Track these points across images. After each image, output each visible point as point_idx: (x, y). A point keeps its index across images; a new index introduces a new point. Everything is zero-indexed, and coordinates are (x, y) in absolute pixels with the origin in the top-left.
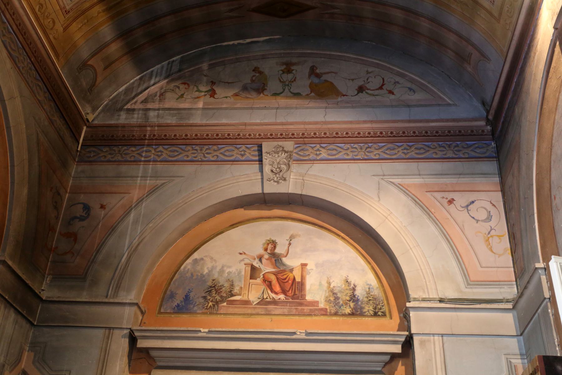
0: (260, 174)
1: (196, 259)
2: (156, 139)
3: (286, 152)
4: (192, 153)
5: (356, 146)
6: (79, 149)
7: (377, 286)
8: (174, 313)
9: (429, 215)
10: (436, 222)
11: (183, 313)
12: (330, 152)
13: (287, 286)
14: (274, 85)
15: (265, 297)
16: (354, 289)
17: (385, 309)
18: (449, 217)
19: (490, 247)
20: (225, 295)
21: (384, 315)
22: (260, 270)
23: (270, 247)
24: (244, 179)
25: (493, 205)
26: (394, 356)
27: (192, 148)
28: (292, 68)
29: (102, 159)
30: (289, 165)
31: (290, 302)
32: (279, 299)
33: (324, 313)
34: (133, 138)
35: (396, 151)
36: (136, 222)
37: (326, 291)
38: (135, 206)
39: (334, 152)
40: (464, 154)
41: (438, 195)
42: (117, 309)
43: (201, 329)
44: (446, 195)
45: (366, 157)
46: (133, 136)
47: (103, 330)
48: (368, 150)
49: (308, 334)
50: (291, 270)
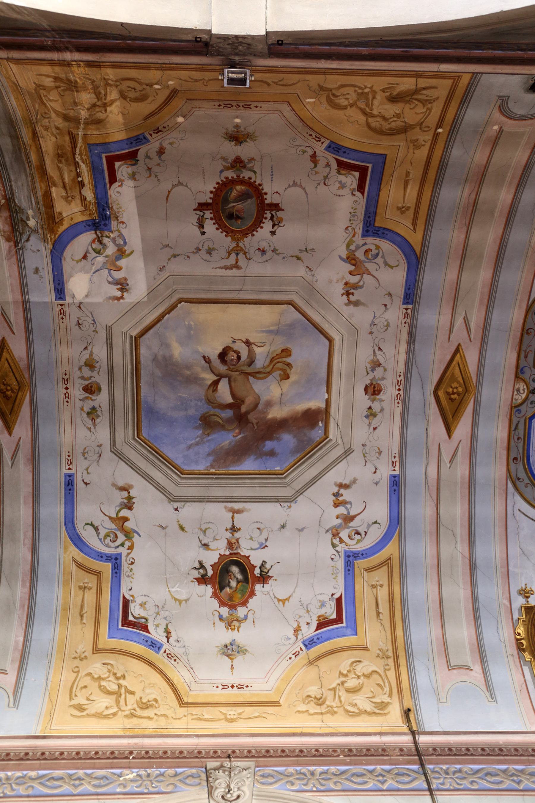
34: (283, 755)
40: (335, 783)
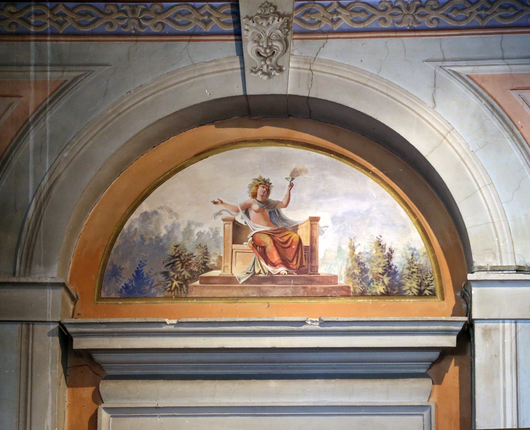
1: (146, 213)
7: (425, 250)
9: (512, 130)
12: (355, 15)
13: (290, 254)
15: (257, 271)
17: (435, 285)
20: (196, 269)
21: (433, 294)
22: (246, 228)
23: (261, 190)
26: (445, 353)
27: (117, 7)
30: (286, 40)
31: (294, 278)
32: (279, 274)
35: (466, 13)
36: (40, 149)
38: (34, 120)
39: (362, 16)
45: (415, 26)
47: (17, 326)
49: (323, 323)
50: (295, 228)
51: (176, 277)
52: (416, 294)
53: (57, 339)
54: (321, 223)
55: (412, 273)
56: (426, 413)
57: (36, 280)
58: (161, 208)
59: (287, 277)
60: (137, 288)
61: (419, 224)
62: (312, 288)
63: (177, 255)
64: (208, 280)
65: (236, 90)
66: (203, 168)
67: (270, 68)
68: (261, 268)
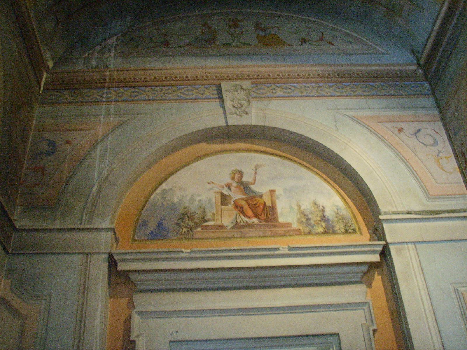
0: (221, 109)
1: (165, 190)
2: (117, 82)
3: (244, 90)
4: (153, 94)
5: (308, 85)
6: (41, 92)
7: (344, 206)
8: (149, 239)
9: (384, 141)
10: (390, 146)
11: (158, 240)
12: (284, 90)
13: (259, 210)
14: (223, 38)
15: (238, 221)
16: (323, 210)
17: (355, 226)
18: (402, 143)
19: (440, 166)
20: (198, 221)
21: (355, 232)
22: (230, 197)
23: (237, 176)
24: (207, 115)
25: (437, 133)
26: (373, 266)
27: (152, 89)
28: (239, 23)
29: (65, 101)
30: (249, 100)
31: (264, 225)
32: (253, 222)
33: (299, 233)
35: (345, 90)
36: (103, 154)
37: (297, 213)
38: (102, 140)
39: (290, 91)
41: (389, 125)
42: (92, 235)
43: (183, 250)
44: (395, 125)
45: (319, 95)
46: (93, 80)
47: (81, 256)
48: (320, 88)
49: (291, 249)
50: (261, 196)
51: (185, 226)
52: (344, 232)
53: (106, 264)
54: (277, 193)
55: (339, 220)
56: (366, 308)
57: (96, 226)
58: (175, 187)
59: (259, 225)
60: (159, 233)
61: (337, 191)
62: (276, 231)
63: (185, 213)
64: (207, 227)
65: (222, 123)
66: (200, 165)
67: (241, 112)
68: (241, 220)
